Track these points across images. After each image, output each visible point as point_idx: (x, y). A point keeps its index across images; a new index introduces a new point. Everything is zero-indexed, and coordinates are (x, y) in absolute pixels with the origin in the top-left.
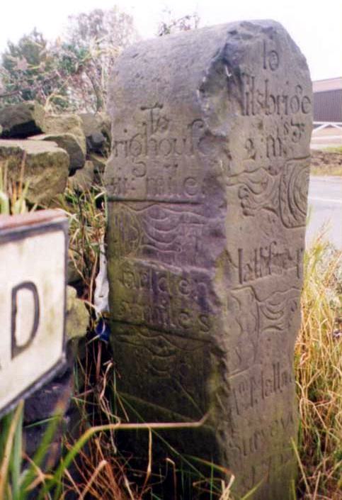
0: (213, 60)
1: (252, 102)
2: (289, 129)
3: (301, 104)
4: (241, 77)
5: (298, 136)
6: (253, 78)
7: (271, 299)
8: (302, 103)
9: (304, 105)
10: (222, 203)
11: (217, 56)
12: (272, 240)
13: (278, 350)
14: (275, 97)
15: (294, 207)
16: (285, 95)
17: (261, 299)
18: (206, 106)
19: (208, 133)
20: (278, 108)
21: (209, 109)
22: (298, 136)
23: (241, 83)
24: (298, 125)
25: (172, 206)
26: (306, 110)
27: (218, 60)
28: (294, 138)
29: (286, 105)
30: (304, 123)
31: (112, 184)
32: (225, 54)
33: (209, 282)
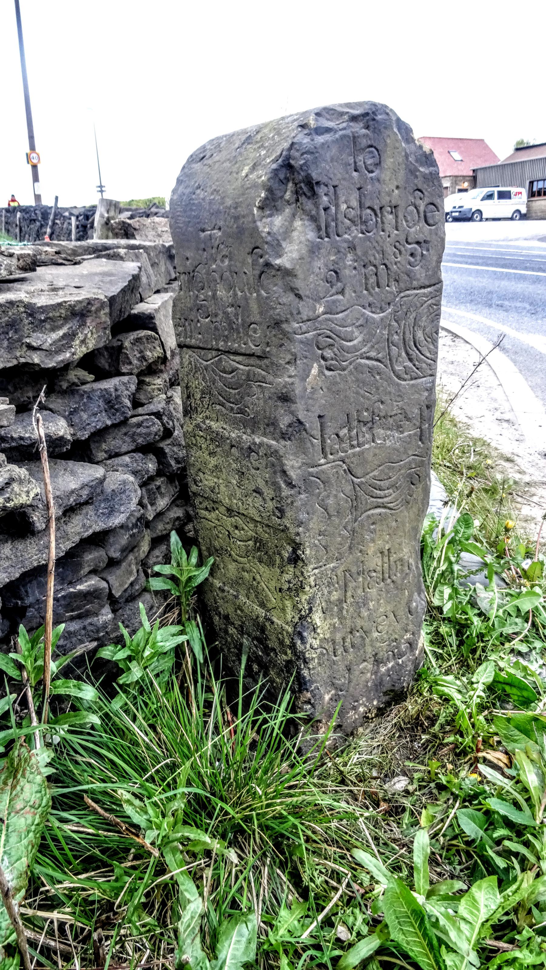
0: (274, 166)
1: (336, 220)
2: (403, 249)
3: (422, 215)
4: (315, 188)
5: (418, 258)
6: (335, 187)
7: (376, 473)
8: (425, 212)
9: (429, 215)
10: (289, 357)
11: (280, 161)
12: (376, 398)
13: (301, 582)
14: (376, 208)
15: (414, 352)
16: (394, 203)
17: (359, 475)
18: (263, 227)
19: (268, 265)
20: (383, 222)
21: (269, 233)
22: (418, 258)
23: (314, 194)
24: (418, 243)
25: (239, 358)
26: (431, 221)
27: (281, 166)
28: (412, 259)
29: (397, 217)
30: (428, 239)
31: (277, 324)
32: (288, 158)
33: (279, 458)
